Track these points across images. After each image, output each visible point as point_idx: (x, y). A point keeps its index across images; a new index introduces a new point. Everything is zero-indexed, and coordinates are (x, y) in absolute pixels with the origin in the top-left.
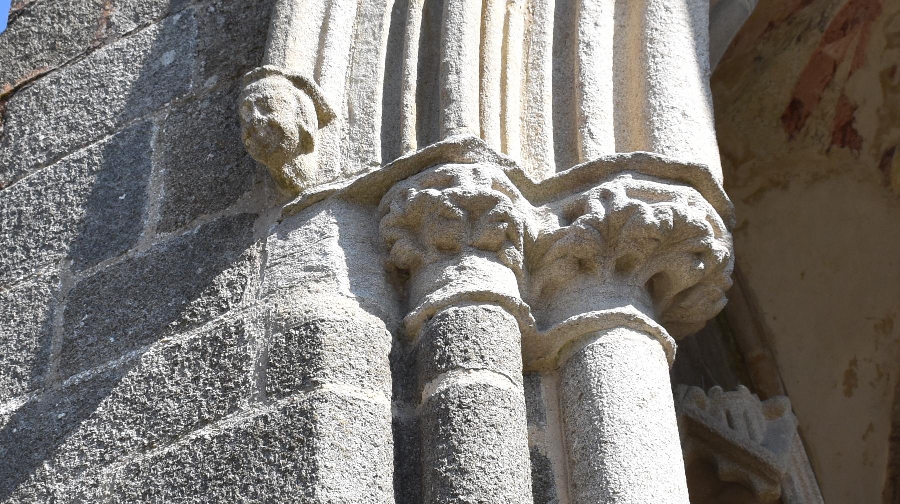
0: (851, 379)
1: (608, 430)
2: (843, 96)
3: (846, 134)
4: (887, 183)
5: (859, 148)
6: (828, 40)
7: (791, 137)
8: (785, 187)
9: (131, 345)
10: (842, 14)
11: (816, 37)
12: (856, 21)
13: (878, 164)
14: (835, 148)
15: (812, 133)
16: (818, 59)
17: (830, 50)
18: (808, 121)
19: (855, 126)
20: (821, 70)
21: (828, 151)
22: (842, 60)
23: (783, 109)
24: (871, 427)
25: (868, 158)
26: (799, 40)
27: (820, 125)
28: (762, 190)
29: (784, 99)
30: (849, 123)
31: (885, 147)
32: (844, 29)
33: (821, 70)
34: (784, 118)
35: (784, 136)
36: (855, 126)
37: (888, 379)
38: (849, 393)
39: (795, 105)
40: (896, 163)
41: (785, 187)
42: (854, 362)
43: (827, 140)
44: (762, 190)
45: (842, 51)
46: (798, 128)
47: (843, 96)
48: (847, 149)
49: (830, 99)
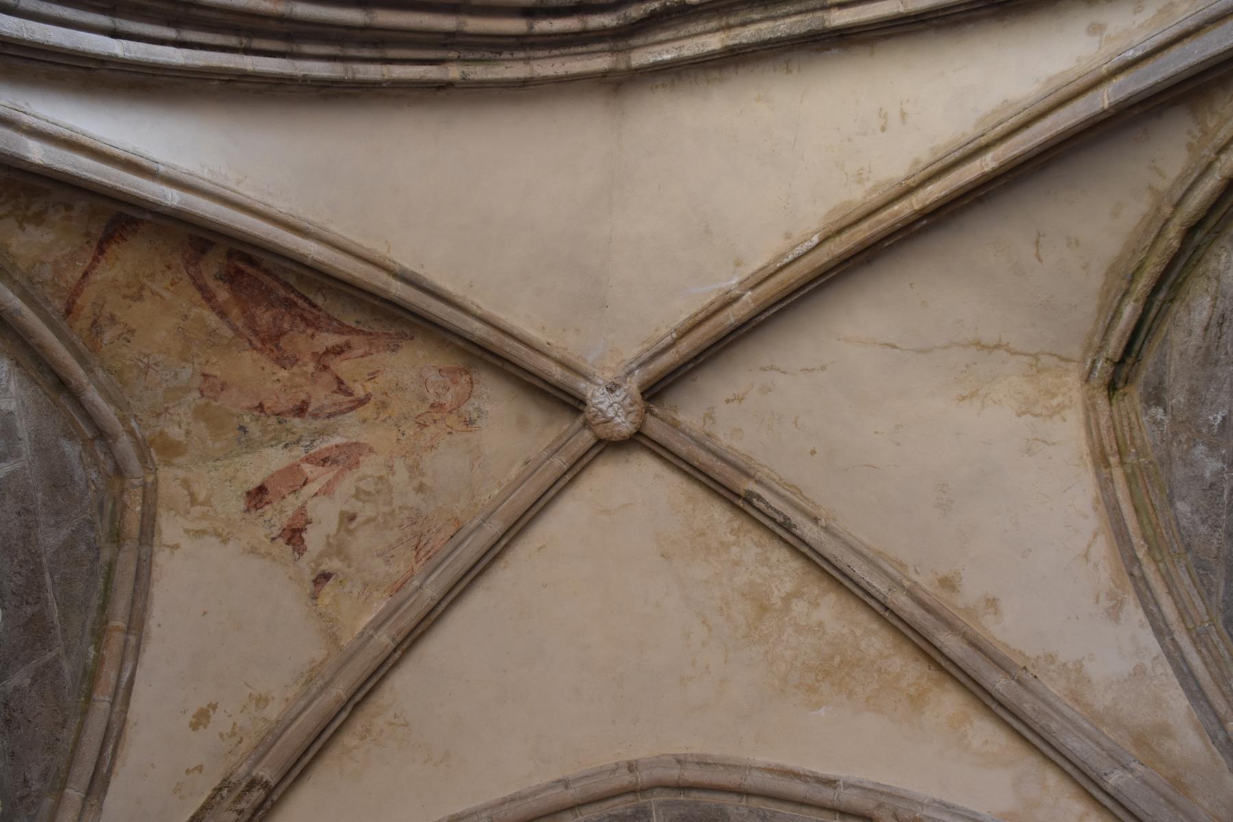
0: (201, 719)
1: (154, 575)
2: (303, 507)
3: (294, 535)
4: (315, 597)
5: (301, 554)
6: (307, 460)
7: (248, 510)
8: (225, 542)
9: (128, 336)
10: (327, 449)
11: (299, 452)
12: (335, 462)
13: (313, 577)
14: (281, 541)
15: (267, 517)
16: (293, 469)
17: (307, 468)
18: (267, 507)
19: (304, 535)
20: (293, 478)
21: (273, 539)
22: (313, 481)
23: (252, 486)
24: (200, 768)
25: (306, 566)
26: (286, 446)
27: (279, 514)
28: (204, 532)
29: (256, 481)
30: (301, 530)
31: (323, 568)
32: (325, 461)
33: (293, 478)
34: (249, 493)
35: (243, 506)
36: (304, 535)
37: (240, 742)
38: (194, 726)
39: (261, 489)
40: (329, 588)
41: (225, 542)
42: (214, 707)
43: (276, 532)
44: (204, 532)
45: (319, 476)
46: (256, 507)
47: (303, 507)
48: (290, 548)
49: (291, 504)
